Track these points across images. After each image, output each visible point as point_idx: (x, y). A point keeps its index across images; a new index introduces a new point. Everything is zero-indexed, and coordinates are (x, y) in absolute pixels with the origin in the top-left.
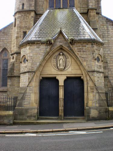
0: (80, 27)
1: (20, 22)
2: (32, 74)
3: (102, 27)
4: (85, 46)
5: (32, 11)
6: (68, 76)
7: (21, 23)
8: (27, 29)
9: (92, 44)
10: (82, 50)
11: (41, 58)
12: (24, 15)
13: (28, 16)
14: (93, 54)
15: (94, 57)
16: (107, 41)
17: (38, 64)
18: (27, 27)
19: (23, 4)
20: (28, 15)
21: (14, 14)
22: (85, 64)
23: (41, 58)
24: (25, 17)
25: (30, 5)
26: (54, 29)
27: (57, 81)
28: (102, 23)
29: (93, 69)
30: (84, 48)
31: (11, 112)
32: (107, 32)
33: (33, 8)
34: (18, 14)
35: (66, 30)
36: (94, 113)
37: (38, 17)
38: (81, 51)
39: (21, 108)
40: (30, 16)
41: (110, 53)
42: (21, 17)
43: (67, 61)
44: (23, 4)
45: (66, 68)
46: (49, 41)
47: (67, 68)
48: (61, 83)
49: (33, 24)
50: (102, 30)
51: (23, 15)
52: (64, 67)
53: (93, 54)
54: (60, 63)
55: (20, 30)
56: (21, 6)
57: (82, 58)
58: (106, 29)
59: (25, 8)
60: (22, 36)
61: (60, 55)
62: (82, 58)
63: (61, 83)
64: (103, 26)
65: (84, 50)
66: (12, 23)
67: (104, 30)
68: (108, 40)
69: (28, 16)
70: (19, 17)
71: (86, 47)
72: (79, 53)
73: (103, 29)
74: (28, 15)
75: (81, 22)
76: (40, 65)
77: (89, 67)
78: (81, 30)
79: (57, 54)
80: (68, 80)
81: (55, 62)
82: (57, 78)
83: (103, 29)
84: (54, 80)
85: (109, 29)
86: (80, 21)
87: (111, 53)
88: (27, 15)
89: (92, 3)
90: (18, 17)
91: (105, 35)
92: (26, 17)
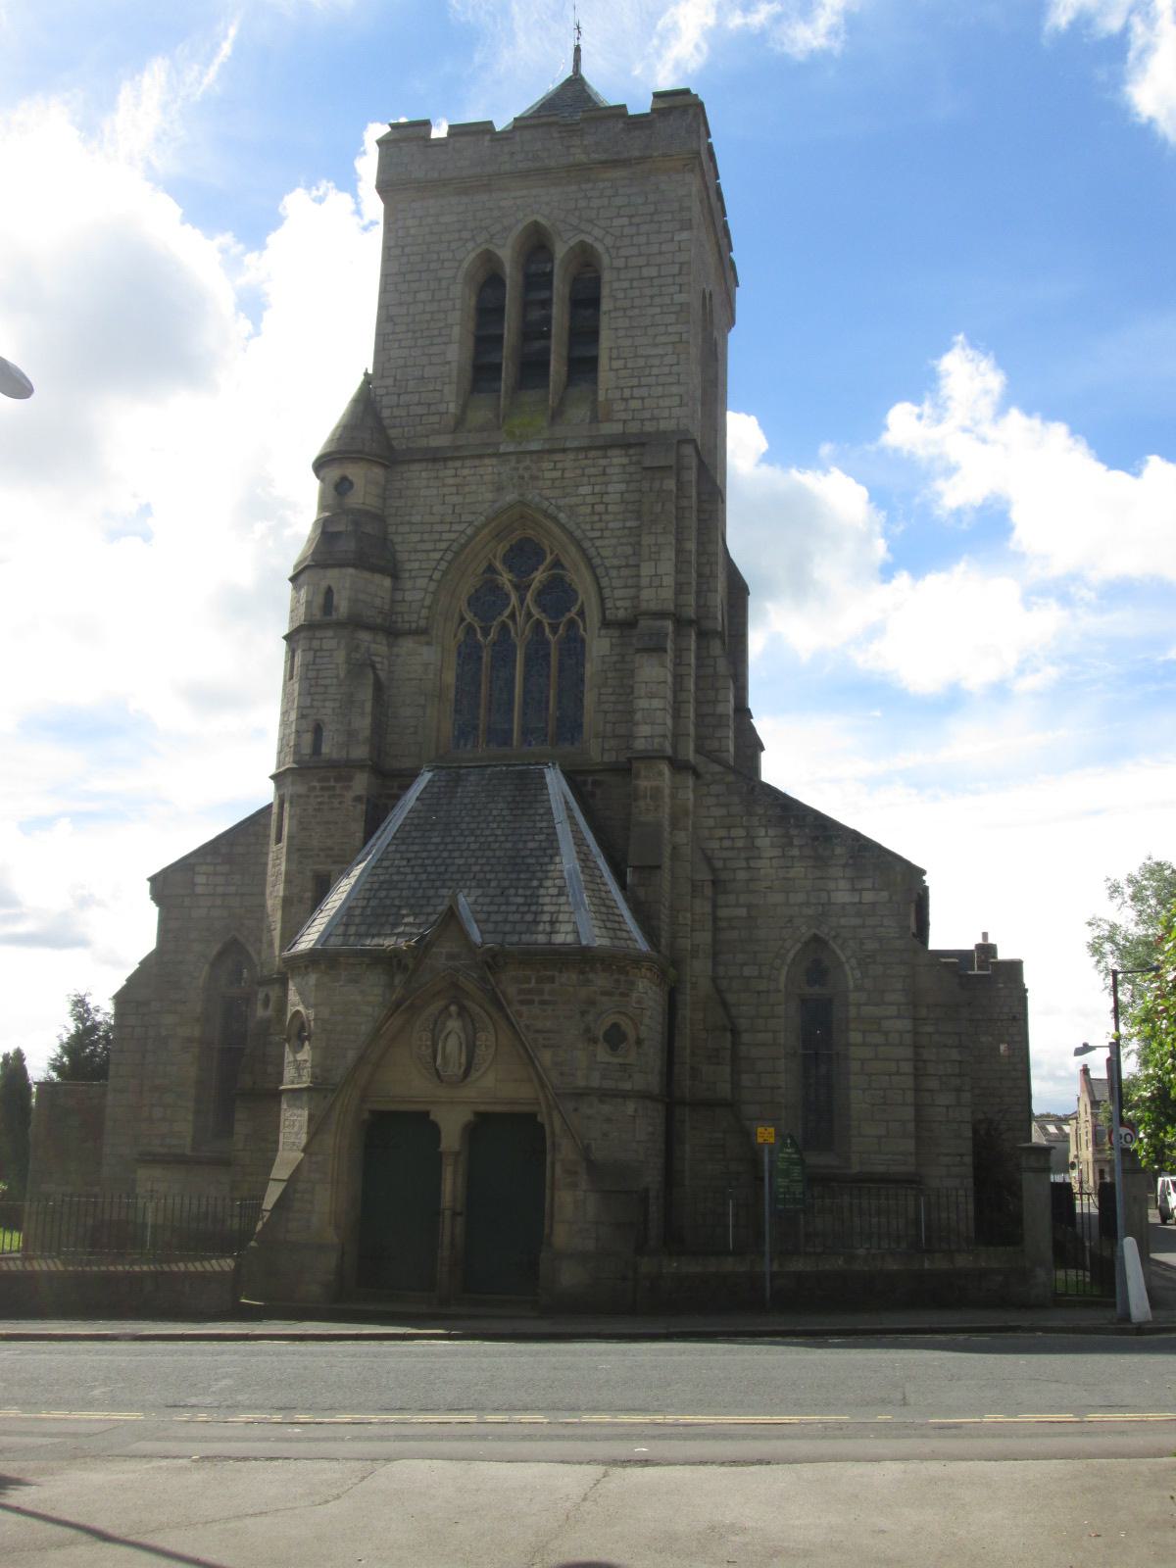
0: (547, 878)
1: (301, 823)
2: (325, 1097)
3: (722, 833)
4: (552, 980)
5: (359, 765)
6: (482, 1108)
7: (304, 829)
8: (335, 862)
9: (582, 972)
10: (537, 998)
11: (363, 1027)
12: (322, 789)
13: (341, 795)
14: (583, 1013)
15: (588, 1030)
16: (742, 912)
17: (351, 1055)
18: (331, 849)
19: (318, 730)
20: (338, 792)
21: (290, 573)
22: (546, 1057)
23: (363, 1027)
24: (326, 800)
25: (351, 734)
26: (431, 892)
27: (435, 1129)
28: (722, 811)
29: (581, 1083)
30: (547, 987)
31: (228, 1264)
32: (747, 859)
33: (360, 752)
34: (293, 784)
35: (480, 900)
36: (570, 1277)
37: (395, 791)
38: (531, 1002)
39: (264, 1225)
40: (350, 795)
41: (756, 973)
42: (308, 796)
43: (478, 1043)
44: (318, 730)
45: (474, 1075)
46: (396, 957)
47: (478, 1074)
48: (451, 1137)
49: (360, 835)
50: (721, 848)
51: (314, 788)
52: (463, 1069)
53: (583, 1013)
54: (448, 1050)
55: (300, 863)
56: (308, 738)
57: (537, 1031)
58: (740, 844)
59: (325, 749)
60: (308, 894)
61: (450, 1016)
62: (537, 1031)
63: (451, 1137)
64: (729, 828)
65: (546, 997)
66: (270, 806)
67: (733, 848)
68: (749, 906)
69: (341, 795)
70: (300, 796)
71: (553, 982)
72: (524, 1008)
73: (727, 843)
74: (338, 792)
75: (557, 854)
76: (361, 1059)
77: (562, 1074)
78: (547, 900)
79: (440, 1004)
80: (483, 1126)
81: (429, 1043)
82: (432, 1117)
83: (727, 843)
84: (421, 1123)
85: (759, 842)
86: (558, 848)
87: (760, 977)
88: (334, 787)
89: (653, 724)
90: (292, 796)
91: (734, 880)
92: (329, 797)
